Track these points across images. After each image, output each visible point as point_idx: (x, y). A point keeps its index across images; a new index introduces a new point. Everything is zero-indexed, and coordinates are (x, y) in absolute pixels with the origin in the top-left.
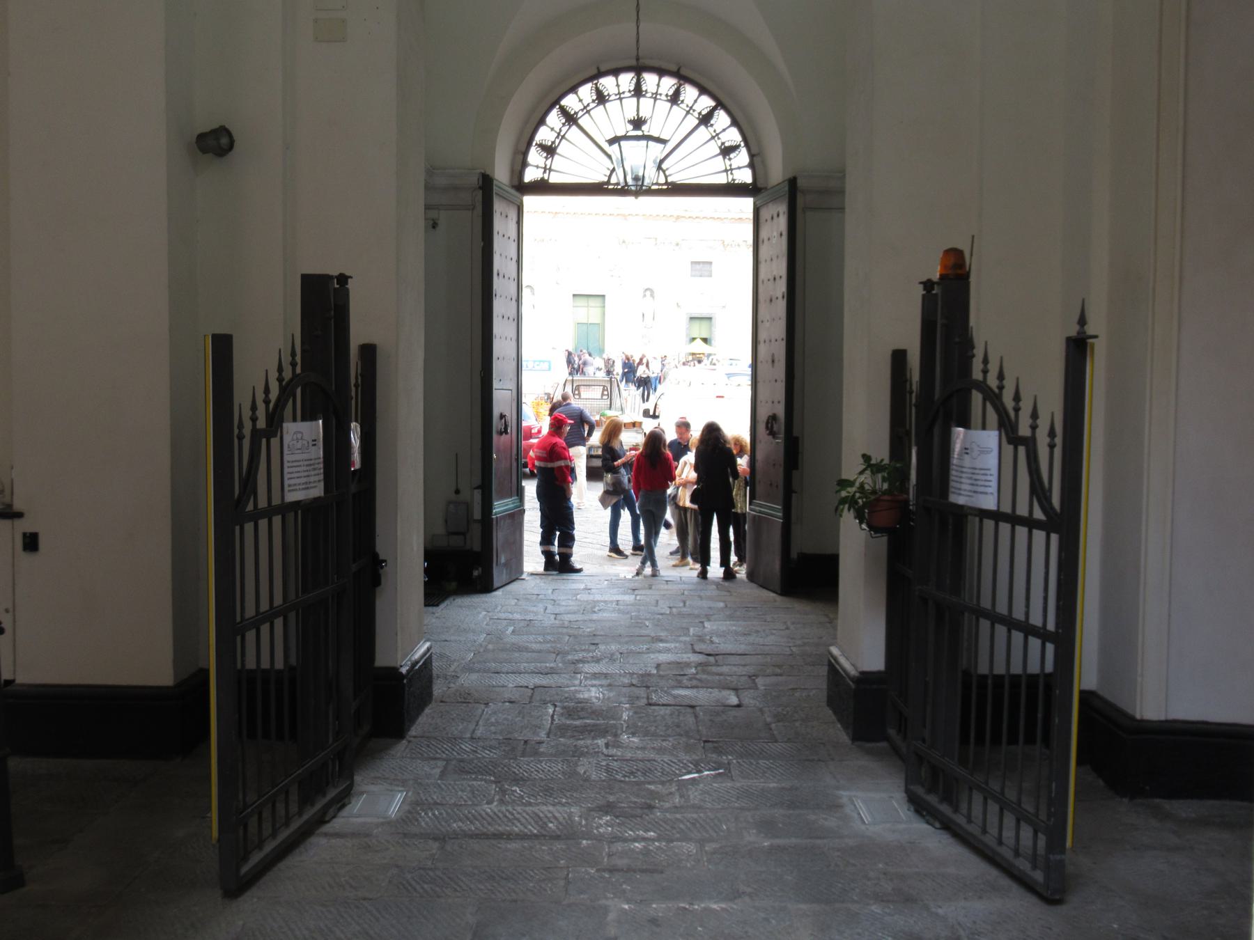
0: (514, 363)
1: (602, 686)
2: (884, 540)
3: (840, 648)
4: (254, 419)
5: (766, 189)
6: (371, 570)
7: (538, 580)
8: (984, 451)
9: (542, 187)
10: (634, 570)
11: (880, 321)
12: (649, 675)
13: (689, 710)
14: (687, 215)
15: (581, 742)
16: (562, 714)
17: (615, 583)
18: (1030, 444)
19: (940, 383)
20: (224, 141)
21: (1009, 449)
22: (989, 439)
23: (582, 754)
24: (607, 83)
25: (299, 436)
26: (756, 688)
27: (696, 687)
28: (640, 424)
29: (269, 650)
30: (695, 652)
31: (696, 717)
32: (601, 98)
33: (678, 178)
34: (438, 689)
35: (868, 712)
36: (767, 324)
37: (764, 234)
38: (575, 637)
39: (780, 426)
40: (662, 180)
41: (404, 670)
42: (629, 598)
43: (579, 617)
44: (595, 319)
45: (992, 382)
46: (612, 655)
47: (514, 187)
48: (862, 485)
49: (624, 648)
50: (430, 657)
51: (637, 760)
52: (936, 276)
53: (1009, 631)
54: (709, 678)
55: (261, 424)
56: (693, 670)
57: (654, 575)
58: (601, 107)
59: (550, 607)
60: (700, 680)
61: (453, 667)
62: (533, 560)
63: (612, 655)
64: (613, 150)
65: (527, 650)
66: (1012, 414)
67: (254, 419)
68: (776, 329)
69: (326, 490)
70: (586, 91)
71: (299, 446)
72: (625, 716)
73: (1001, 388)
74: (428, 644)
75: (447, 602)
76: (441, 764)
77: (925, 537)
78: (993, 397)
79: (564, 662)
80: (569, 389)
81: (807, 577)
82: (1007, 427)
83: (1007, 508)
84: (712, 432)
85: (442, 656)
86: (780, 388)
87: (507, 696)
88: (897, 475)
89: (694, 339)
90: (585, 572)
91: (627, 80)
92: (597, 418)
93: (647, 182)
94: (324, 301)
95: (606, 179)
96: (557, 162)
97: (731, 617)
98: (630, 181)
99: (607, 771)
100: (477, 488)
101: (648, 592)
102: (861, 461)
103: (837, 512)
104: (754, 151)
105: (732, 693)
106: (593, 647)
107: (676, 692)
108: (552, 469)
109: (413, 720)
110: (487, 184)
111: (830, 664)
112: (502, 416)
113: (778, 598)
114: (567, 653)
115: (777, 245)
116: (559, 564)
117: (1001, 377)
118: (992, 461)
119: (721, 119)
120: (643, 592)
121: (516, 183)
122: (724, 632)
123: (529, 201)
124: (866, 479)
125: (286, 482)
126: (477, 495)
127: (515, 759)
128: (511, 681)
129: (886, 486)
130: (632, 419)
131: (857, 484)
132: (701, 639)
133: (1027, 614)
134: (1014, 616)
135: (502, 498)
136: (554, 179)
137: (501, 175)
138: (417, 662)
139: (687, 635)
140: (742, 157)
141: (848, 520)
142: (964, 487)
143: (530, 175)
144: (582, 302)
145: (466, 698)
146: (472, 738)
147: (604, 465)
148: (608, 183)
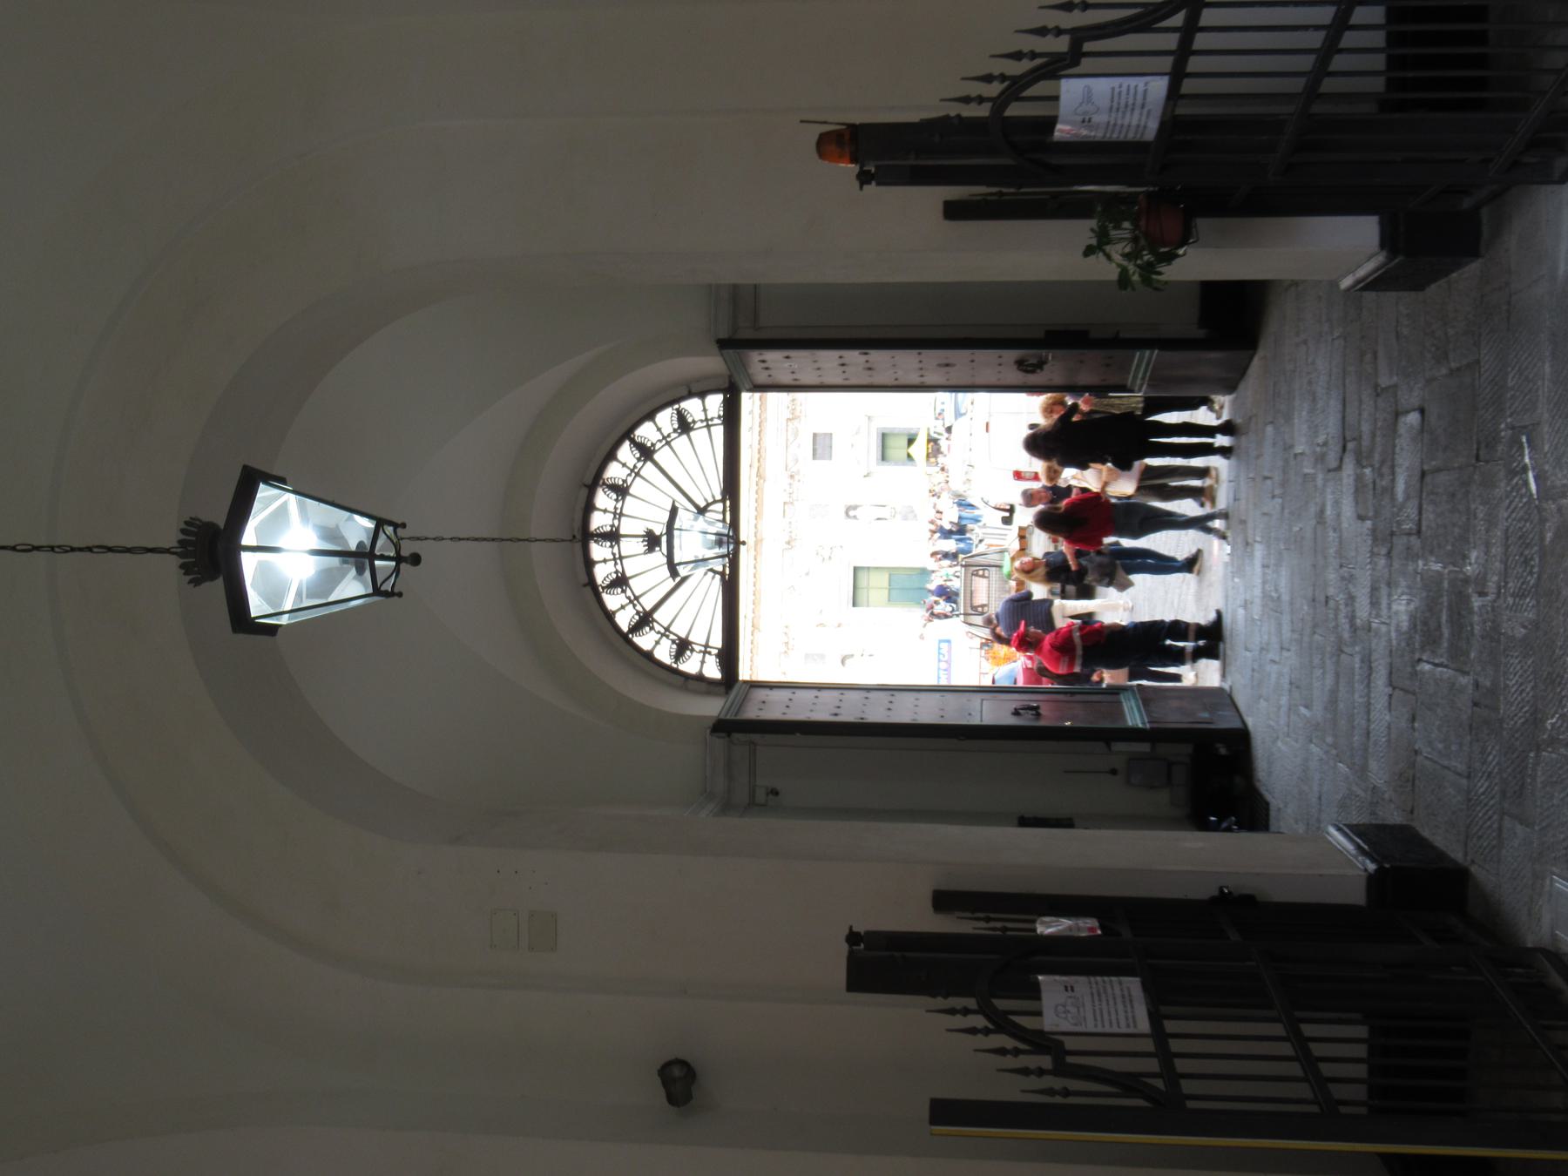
0: (948, 696)
1: (1390, 595)
2: (1203, 224)
3: (1344, 276)
4: (1041, 1072)
5: (730, 377)
6: (1234, 909)
7: (1232, 669)
8: (1088, 96)
9: (729, 656)
10: (1216, 542)
11: (909, 237)
12: (1374, 531)
13: (1428, 479)
14: (756, 465)
15: (1477, 629)
16: (1433, 652)
17: (1238, 565)
18: (1080, 36)
19: (992, 157)
20: (677, 1072)
21: (1086, 64)
22: (1071, 90)
23: (1496, 628)
24: (602, 573)
25: (1060, 1009)
26: (1395, 386)
27: (1393, 467)
28: (1021, 529)
29: (1343, 1045)
30: (1339, 468)
31: (1438, 470)
32: (621, 582)
33: (717, 490)
34: (1395, 817)
35: (1435, 237)
36: (900, 373)
37: (787, 379)
38: (1315, 626)
39: (1030, 354)
40: (719, 507)
41: (1372, 867)
42: (1259, 551)
43: (1286, 619)
44: (883, 580)
45: (995, 89)
46: (1343, 578)
47: (727, 693)
48: (1126, 256)
49: (1335, 563)
50: (1347, 826)
51: (1506, 553)
52: (853, 168)
53: (1340, 51)
54: (1379, 449)
55: (1046, 1061)
56: (1368, 471)
57: (1224, 515)
58: (631, 582)
59: (1271, 656)
60: (1383, 462)
61: (1360, 792)
62: (1202, 674)
63: (1343, 578)
64: (683, 571)
65: (1334, 692)
66: (1038, 61)
67: (1041, 1072)
68: (906, 362)
69: (1131, 973)
70: (612, 601)
71: (1073, 1010)
72: (1438, 567)
73: (1003, 78)
74: (1332, 830)
75: (1263, 790)
76: (1507, 822)
77: (1201, 169)
78: (1015, 88)
79: (1354, 644)
80: (979, 620)
81: (1232, 324)
82: (1056, 67)
83: (1167, 63)
84: (1038, 443)
85: (1343, 806)
86: (981, 355)
87: (1403, 724)
88: (1111, 211)
89: (909, 456)
90: (1220, 605)
91: (598, 551)
92: (1013, 584)
93: (719, 527)
94: (880, 963)
95: (718, 577)
96: (697, 638)
97: (1288, 418)
98: (724, 550)
99: (1523, 596)
100: (1109, 746)
101: (1250, 525)
102: (1092, 258)
103: (1157, 288)
104: (685, 393)
105: (1402, 419)
106: (1332, 603)
107: (1400, 496)
108: (1085, 648)
109: (1441, 855)
110: (724, 727)
111: (1362, 289)
112: (1016, 713)
113: (1260, 353)
114: (1340, 639)
115: (802, 362)
116: (1210, 640)
117: (988, 79)
118: (1102, 86)
119: (646, 432)
120: (1250, 532)
121: (722, 689)
122: (1311, 427)
123: (744, 674)
124: (1117, 251)
125: (1124, 1030)
126: (1119, 746)
127: (1501, 721)
128: (1381, 717)
129: (1126, 225)
130: (1011, 539)
131: (1125, 263)
132: (1320, 459)
133: (1317, 28)
134: (1318, 45)
135: (1120, 714)
136: (717, 641)
137: (712, 707)
138: (1359, 847)
139: (1313, 478)
140: (692, 407)
141: (1172, 272)
142: (1134, 122)
143: (713, 671)
144: (862, 595)
145: (1408, 779)
146: (1469, 777)
147: (1074, 583)
148: (722, 574)
